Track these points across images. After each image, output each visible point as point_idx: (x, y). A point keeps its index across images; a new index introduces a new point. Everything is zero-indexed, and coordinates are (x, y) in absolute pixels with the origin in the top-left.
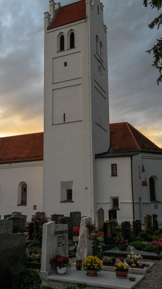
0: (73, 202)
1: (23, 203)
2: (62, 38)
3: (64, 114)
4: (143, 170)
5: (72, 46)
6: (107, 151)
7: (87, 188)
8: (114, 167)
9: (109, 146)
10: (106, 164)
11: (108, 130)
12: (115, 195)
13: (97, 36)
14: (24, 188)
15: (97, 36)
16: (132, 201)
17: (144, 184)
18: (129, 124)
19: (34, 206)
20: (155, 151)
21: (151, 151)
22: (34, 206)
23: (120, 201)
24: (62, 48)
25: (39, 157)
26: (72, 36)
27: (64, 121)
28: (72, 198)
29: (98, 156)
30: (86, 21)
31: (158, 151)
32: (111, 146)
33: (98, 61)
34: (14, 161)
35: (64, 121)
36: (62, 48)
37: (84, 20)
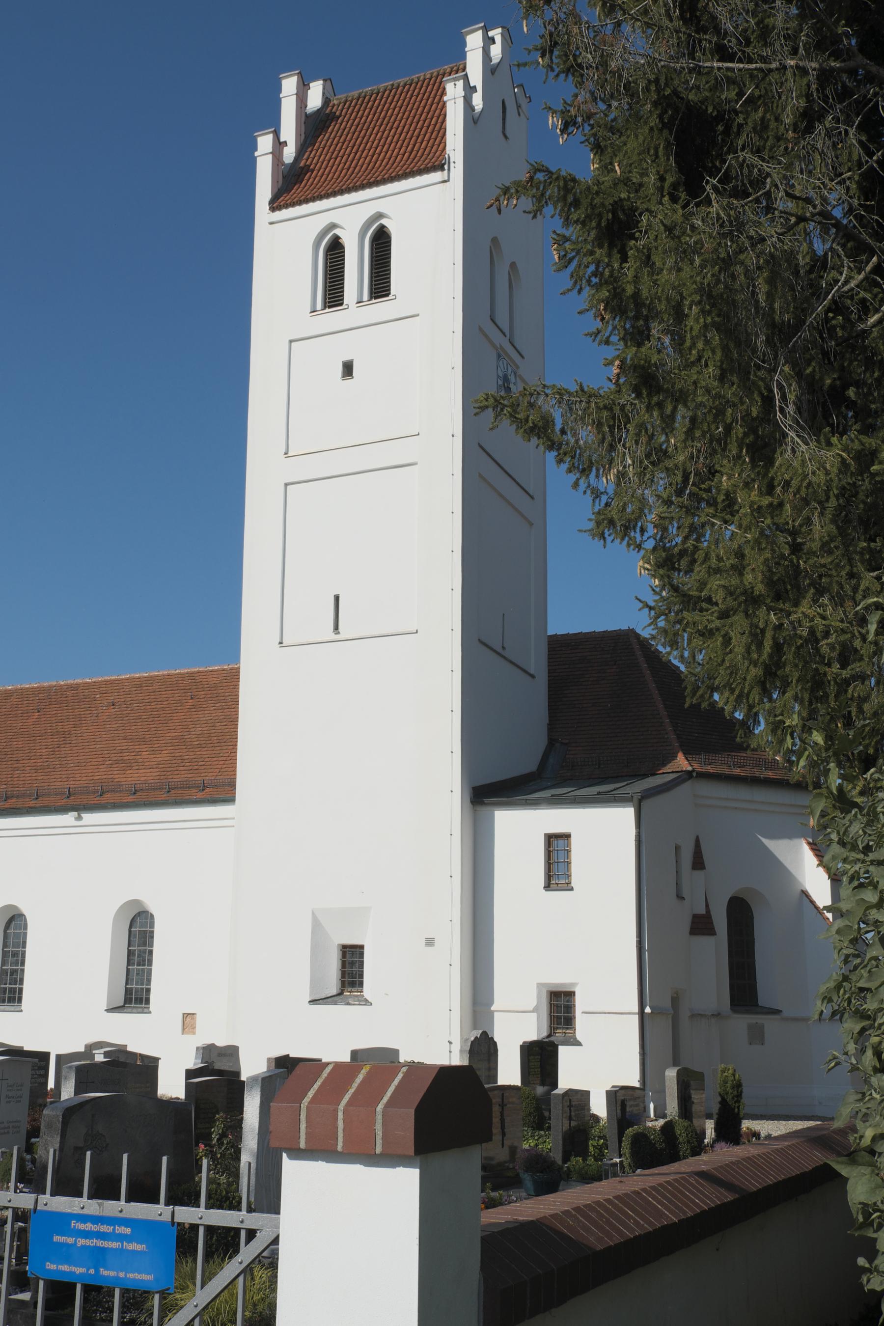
0: (367, 1003)
1: (134, 997)
2: (335, 251)
3: (337, 598)
4: (698, 863)
5: (380, 286)
6: (530, 765)
7: (430, 942)
8: (556, 846)
9: (542, 742)
10: (521, 829)
11: (537, 661)
12: (559, 978)
13: (495, 241)
14: (138, 934)
15: (495, 241)
16: (636, 1009)
17: (701, 925)
19: (186, 1016)
21: (737, 771)
22: (186, 1016)
23: (580, 1005)
24: (333, 295)
26: (381, 242)
27: (336, 627)
29: (488, 791)
30: (448, 181)
31: (770, 774)
32: (551, 742)
33: (499, 356)
35: (336, 627)
36: (333, 295)
37: (436, 176)
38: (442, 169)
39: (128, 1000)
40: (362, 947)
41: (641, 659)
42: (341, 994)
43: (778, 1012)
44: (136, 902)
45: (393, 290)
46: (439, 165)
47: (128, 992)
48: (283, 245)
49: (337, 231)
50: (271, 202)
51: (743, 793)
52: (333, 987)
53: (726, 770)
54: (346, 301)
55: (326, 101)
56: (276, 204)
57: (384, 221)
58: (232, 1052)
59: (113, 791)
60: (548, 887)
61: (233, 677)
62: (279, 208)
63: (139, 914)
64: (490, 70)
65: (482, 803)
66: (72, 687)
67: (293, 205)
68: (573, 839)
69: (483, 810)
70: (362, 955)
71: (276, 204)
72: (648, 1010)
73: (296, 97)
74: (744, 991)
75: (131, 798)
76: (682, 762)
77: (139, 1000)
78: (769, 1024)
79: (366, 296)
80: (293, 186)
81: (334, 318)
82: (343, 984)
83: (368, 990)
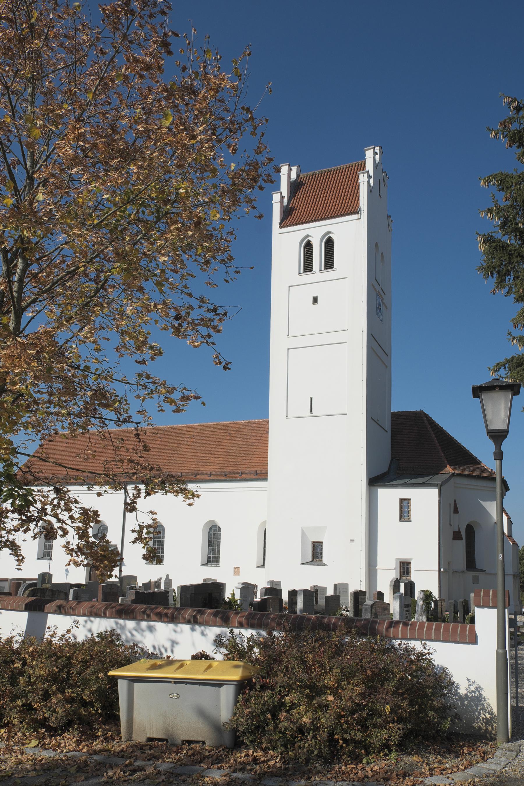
0: (325, 565)
1: (212, 558)
2: (308, 247)
3: (311, 399)
5: (329, 264)
6: (385, 469)
7: (352, 541)
8: (405, 506)
10: (389, 497)
12: (405, 557)
14: (213, 534)
16: (437, 569)
17: (457, 536)
18: (426, 416)
19: (235, 568)
20: (479, 474)
21: (471, 473)
22: (235, 568)
23: (413, 567)
24: (308, 267)
25: (409, 563)
26: (329, 244)
27: (311, 411)
28: (321, 557)
29: (376, 480)
31: (484, 475)
34: (194, 479)
35: (311, 411)
36: (308, 267)
37: (355, 216)
38: (358, 213)
39: (209, 561)
40: (322, 543)
41: (426, 421)
42: (312, 561)
43: (484, 571)
44: (213, 521)
45: (335, 265)
46: (356, 211)
47: (209, 558)
48: (286, 244)
49: (309, 238)
50: (280, 224)
51: (473, 482)
52: (310, 559)
53: (467, 473)
54: (314, 270)
55: (298, 176)
56: (282, 225)
57: (331, 235)
58: (279, 583)
59: (201, 475)
60: (400, 520)
61: (262, 430)
62: (284, 227)
63: (213, 526)
64: (376, 166)
65: (374, 485)
66: (174, 429)
67: (290, 226)
68: (412, 502)
69: (373, 488)
70: (322, 546)
71: (282, 225)
72: (442, 570)
73: (287, 174)
74: (471, 563)
75: (209, 478)
76: (449, 469)
77: (317, 557)
78: (481, 575)
79: (323, 268)
80: (289, 217)
81: (308, 277)
82: (313, 557)
83: (325, 560)
